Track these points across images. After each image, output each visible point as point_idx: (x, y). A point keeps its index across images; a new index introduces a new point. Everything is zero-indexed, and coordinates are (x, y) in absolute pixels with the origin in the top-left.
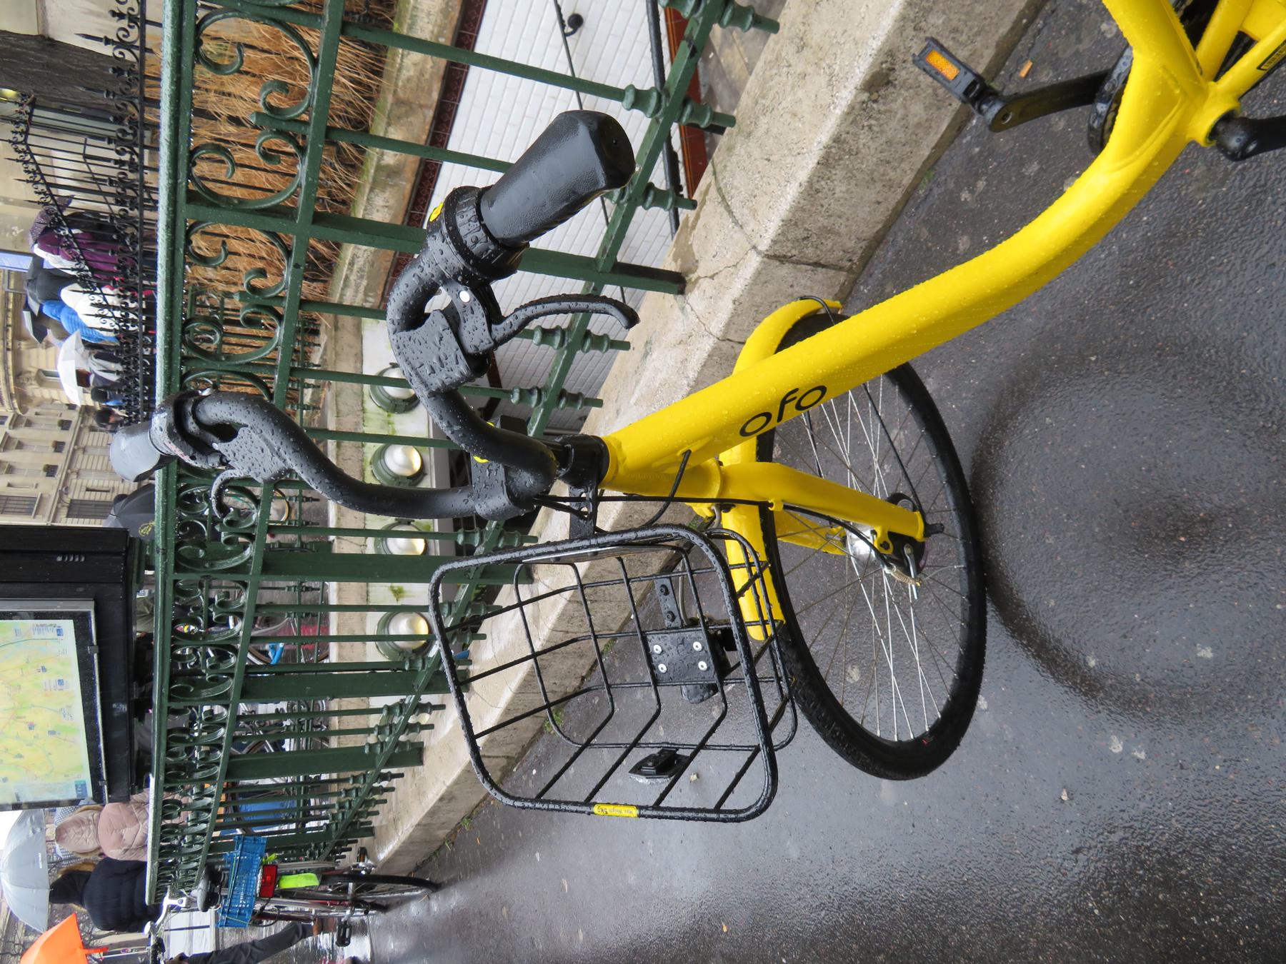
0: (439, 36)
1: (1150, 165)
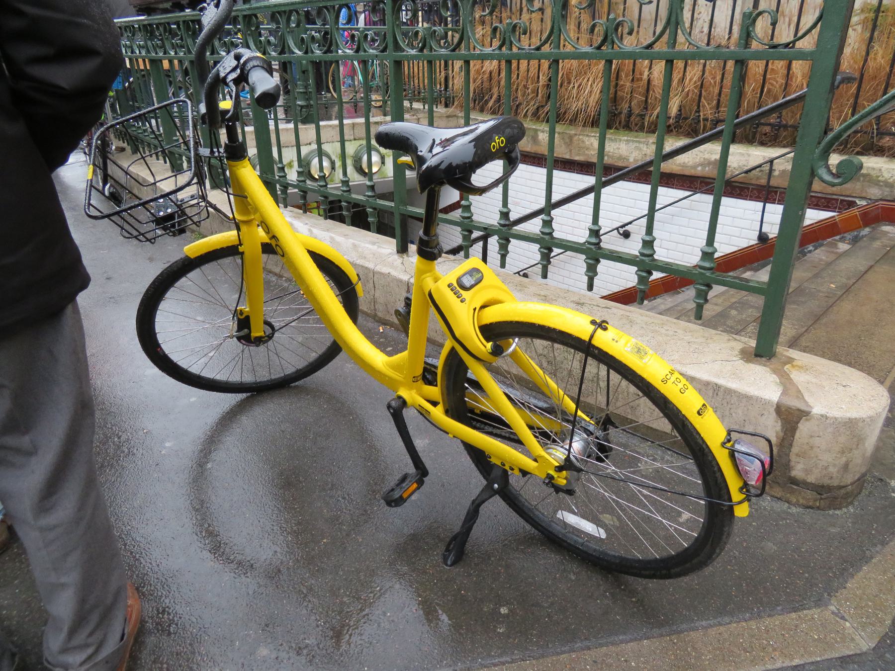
0: (608, 156)
1: (386, 376)
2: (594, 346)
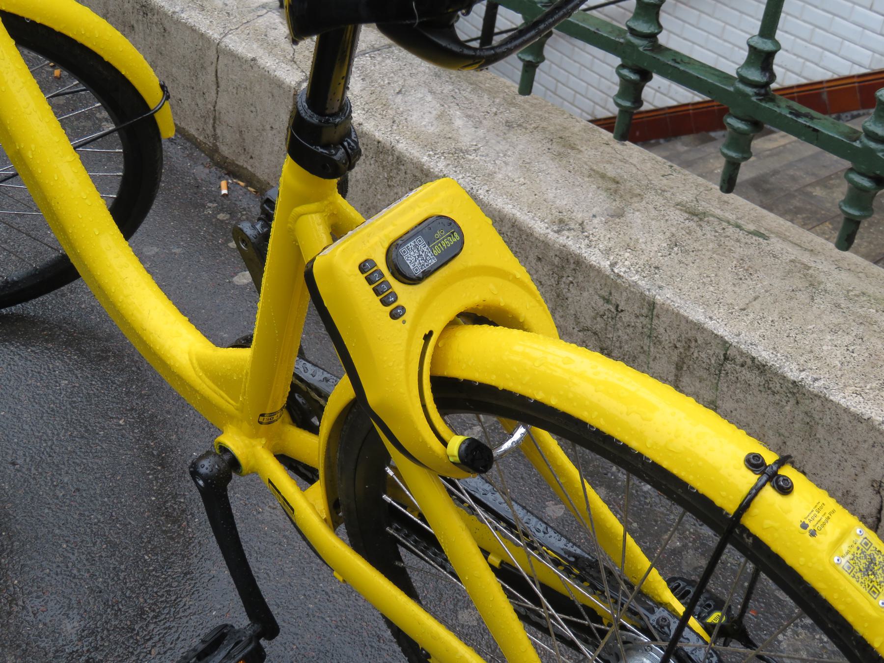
2: (745, 530)
